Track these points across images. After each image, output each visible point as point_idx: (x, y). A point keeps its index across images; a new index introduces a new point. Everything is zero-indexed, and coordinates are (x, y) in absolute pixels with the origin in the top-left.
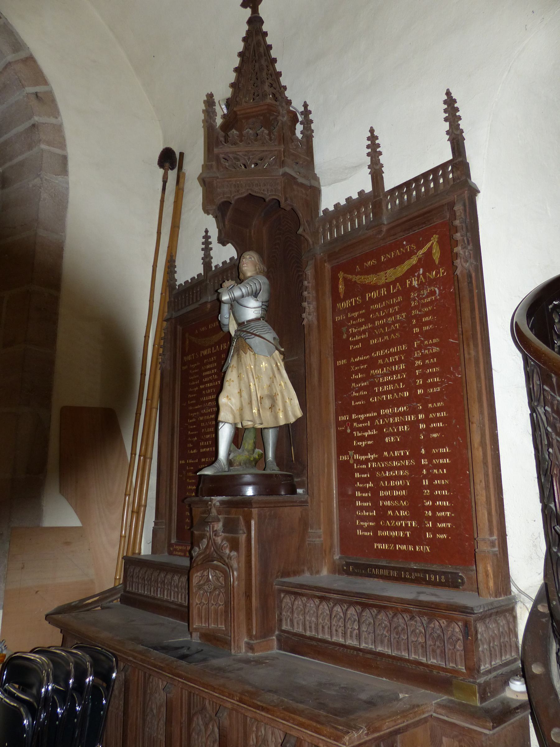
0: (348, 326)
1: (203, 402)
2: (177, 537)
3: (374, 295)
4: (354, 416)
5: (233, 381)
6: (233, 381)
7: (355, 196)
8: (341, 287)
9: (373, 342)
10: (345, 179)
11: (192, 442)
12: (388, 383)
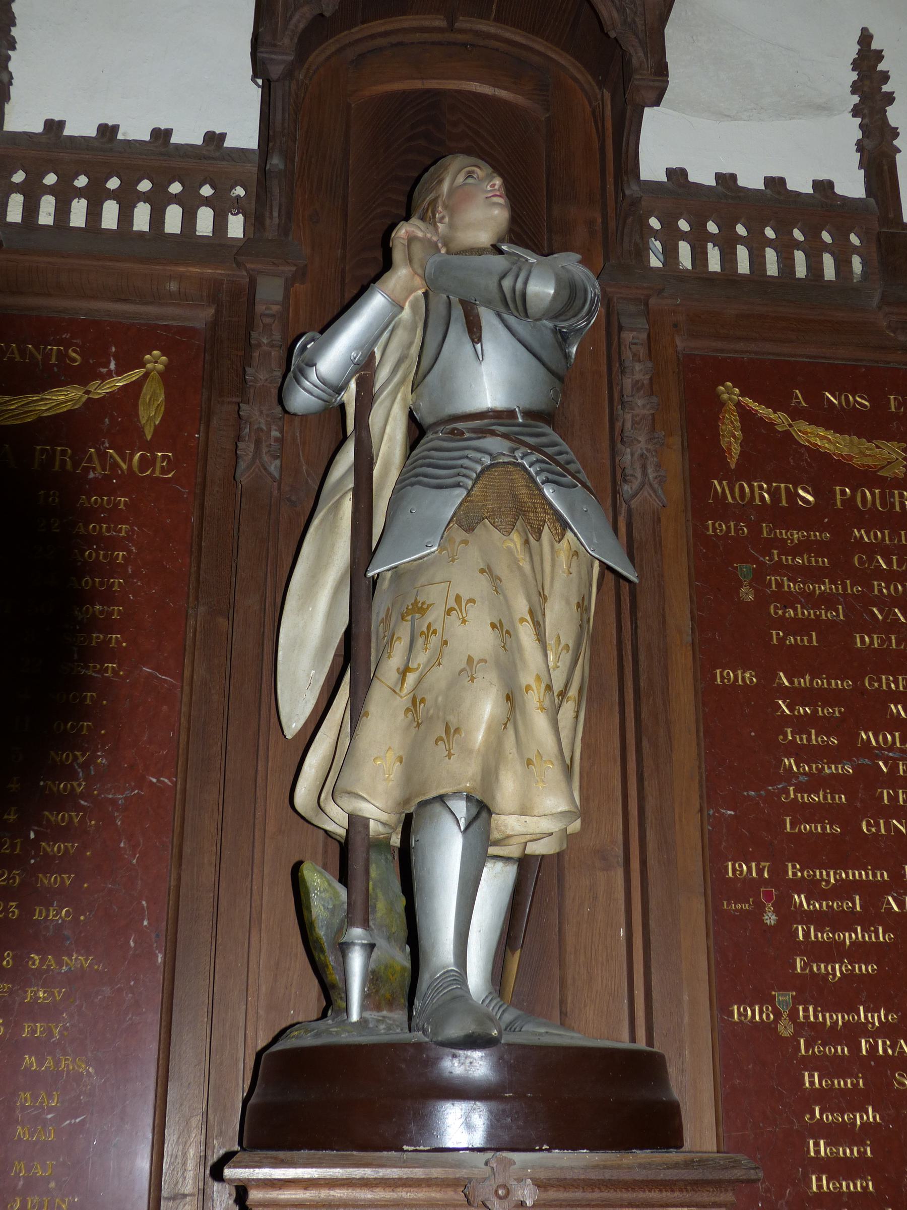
0: (761, 564)
8: (732, 437)
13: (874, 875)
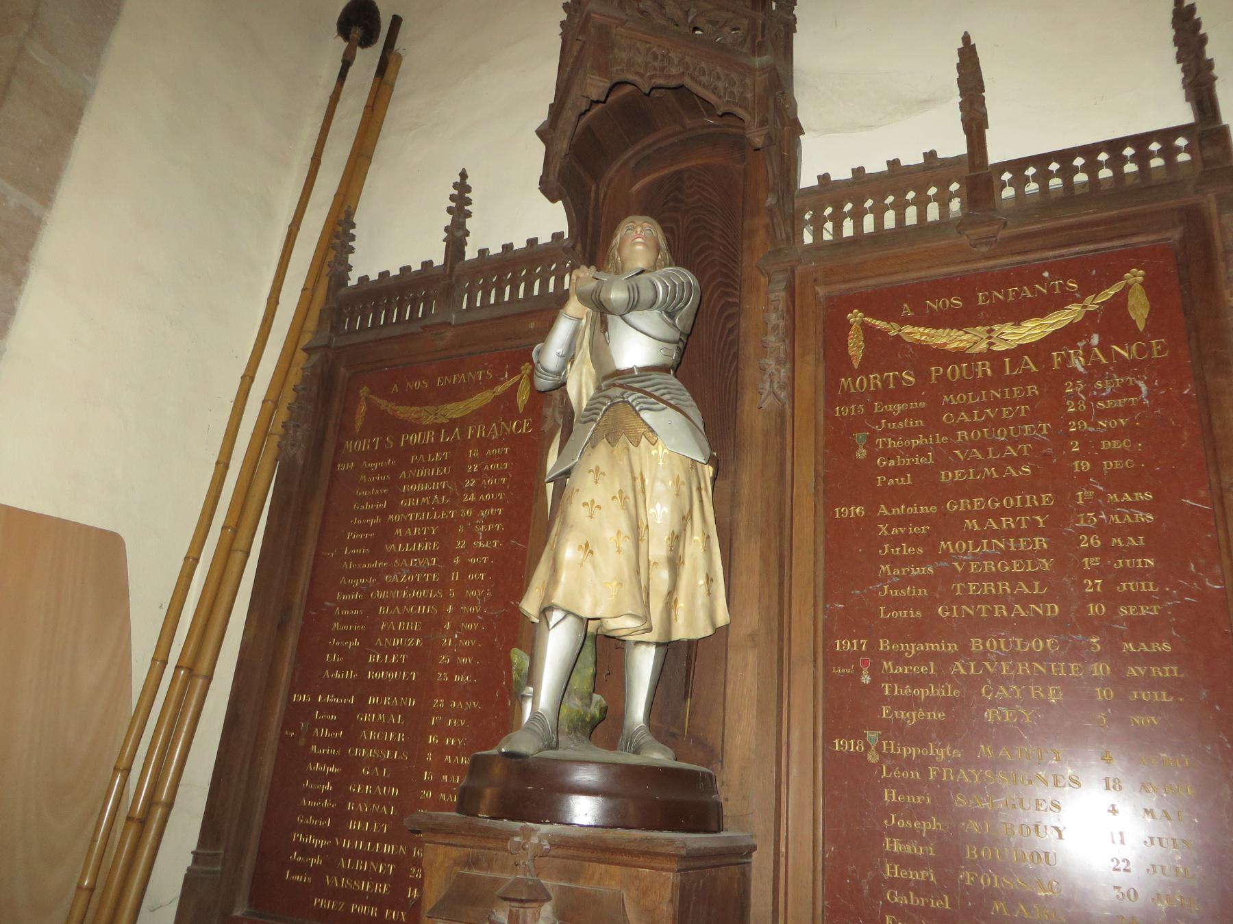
0: (873, 432)
1: (390, 557)
2: (250, 899)
3: (415, 439)
4: (883, 645)
5: (599, 507)
6: (599, 507)
7: (416, 267)
8: (856, 347)
9: (945, 477)
10: (870, 127)
11: (341, 651)
12: (994, 577)
13: (947, 647)
